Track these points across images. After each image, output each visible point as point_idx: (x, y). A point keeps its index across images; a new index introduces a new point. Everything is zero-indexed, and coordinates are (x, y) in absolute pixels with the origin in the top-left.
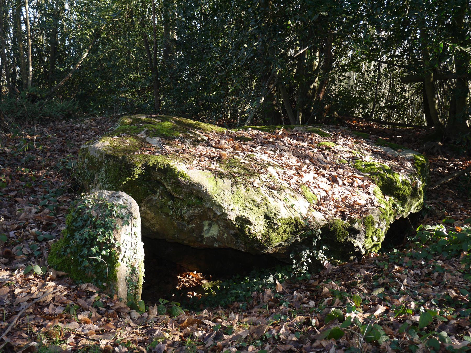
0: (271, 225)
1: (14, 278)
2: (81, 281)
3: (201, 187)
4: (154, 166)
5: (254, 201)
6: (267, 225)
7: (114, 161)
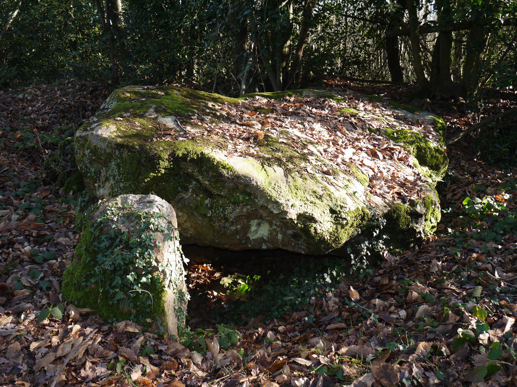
0: (339, 220)
1: (22, 327)
2: (114, 319)
3: (250, 180)
4: (185, 156)
5: (315, 192)
6: (334, 221)
7: (129, 152)
